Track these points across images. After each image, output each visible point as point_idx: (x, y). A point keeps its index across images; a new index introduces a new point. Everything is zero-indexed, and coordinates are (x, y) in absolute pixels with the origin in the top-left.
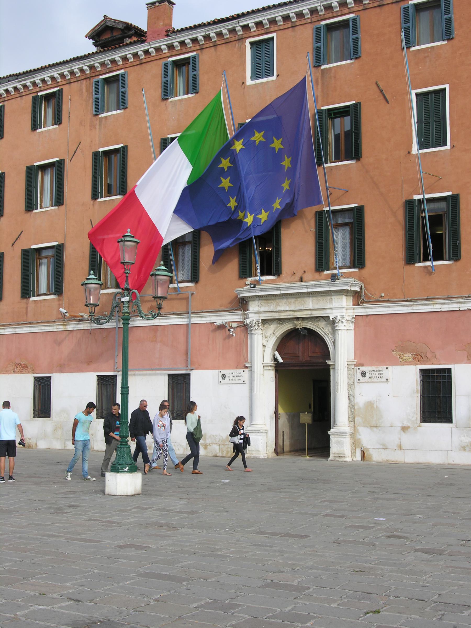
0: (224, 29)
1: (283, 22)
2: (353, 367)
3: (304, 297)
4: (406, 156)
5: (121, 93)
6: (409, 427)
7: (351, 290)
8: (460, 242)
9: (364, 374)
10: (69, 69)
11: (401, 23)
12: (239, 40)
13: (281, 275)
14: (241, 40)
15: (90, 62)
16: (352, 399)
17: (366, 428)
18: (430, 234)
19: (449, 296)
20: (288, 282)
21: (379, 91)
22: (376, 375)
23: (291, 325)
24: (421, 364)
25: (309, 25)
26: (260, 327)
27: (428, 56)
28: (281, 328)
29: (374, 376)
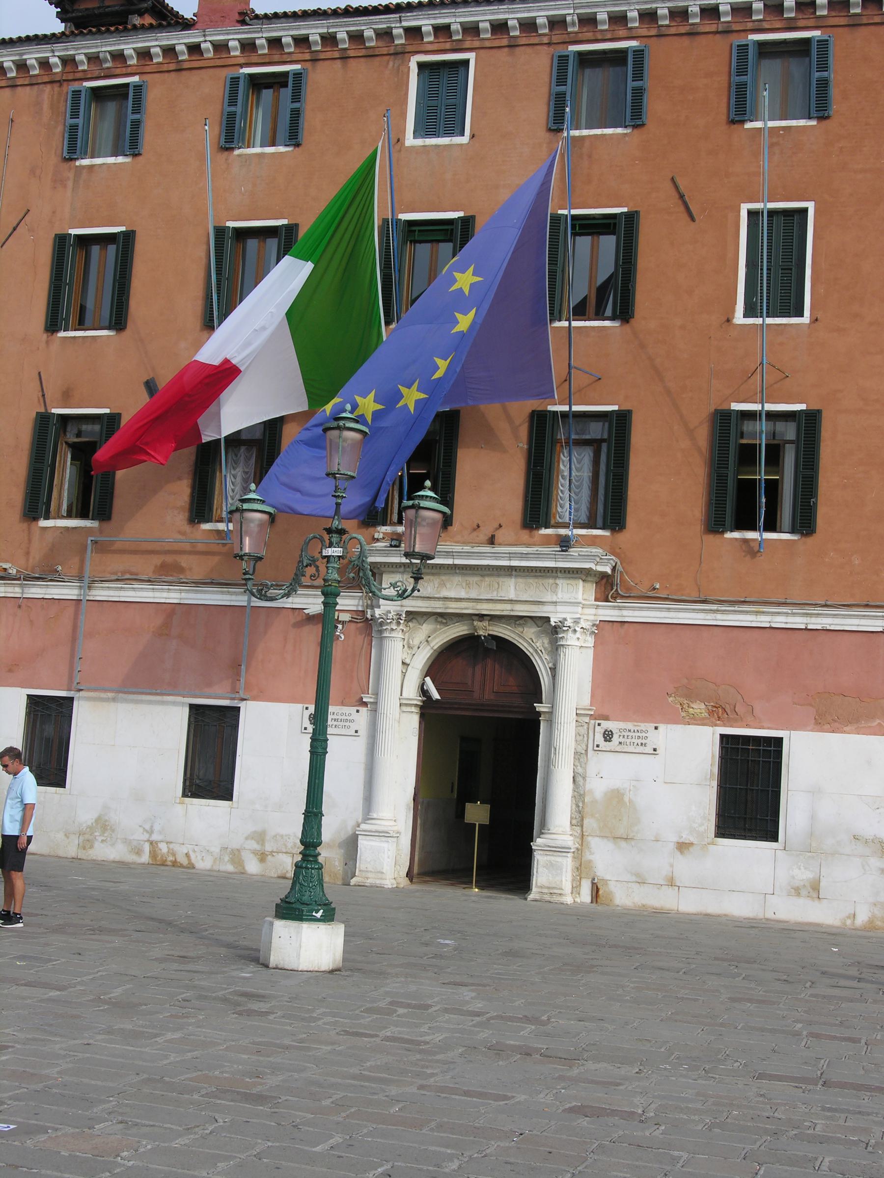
0: (368, 28)
1: (492, 34)
2: (587, 719)
3: (499, 576)
4: (721, 326)
5: (814, 83)
6: (692, 844)
7: (596, 571)
8: (817, 500)
9: (608, 736)
10: (17, 58)
11: (730, 72)
12: (396, 54)
13: (449, 528)
14: (400, 56)
15: (67, 50)
16: (581, 783)
17: (605, 840)
18: (759, 480)
19: (788, 601)
20: (465, 543)
21: (677, 197)
22: (633, 740)
23: (465, 628)
24: (725, 725)
25: (545, 48)
26: (401, 627)
27: (777, 144)
28: (445, 632)
29: (628, 741)
